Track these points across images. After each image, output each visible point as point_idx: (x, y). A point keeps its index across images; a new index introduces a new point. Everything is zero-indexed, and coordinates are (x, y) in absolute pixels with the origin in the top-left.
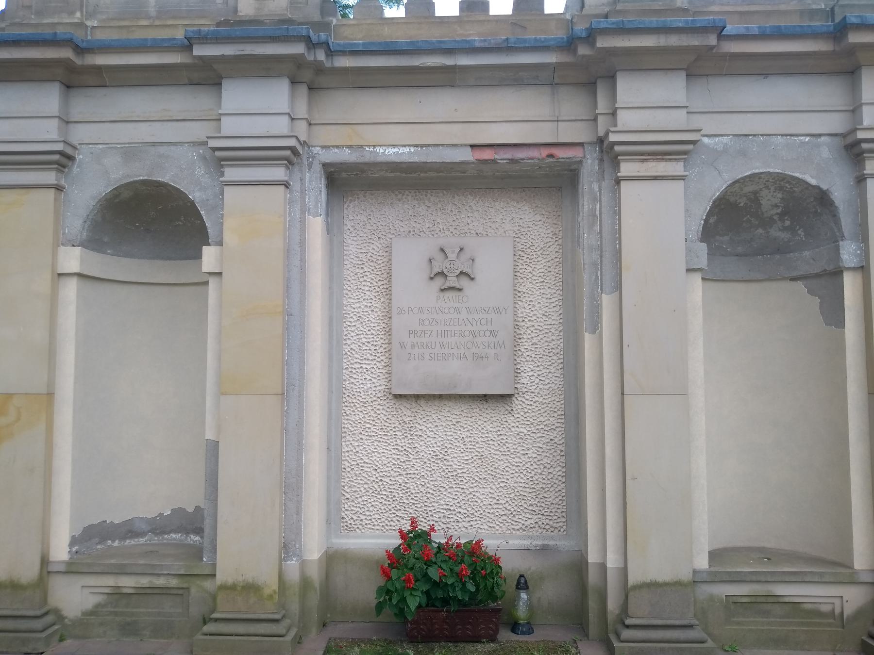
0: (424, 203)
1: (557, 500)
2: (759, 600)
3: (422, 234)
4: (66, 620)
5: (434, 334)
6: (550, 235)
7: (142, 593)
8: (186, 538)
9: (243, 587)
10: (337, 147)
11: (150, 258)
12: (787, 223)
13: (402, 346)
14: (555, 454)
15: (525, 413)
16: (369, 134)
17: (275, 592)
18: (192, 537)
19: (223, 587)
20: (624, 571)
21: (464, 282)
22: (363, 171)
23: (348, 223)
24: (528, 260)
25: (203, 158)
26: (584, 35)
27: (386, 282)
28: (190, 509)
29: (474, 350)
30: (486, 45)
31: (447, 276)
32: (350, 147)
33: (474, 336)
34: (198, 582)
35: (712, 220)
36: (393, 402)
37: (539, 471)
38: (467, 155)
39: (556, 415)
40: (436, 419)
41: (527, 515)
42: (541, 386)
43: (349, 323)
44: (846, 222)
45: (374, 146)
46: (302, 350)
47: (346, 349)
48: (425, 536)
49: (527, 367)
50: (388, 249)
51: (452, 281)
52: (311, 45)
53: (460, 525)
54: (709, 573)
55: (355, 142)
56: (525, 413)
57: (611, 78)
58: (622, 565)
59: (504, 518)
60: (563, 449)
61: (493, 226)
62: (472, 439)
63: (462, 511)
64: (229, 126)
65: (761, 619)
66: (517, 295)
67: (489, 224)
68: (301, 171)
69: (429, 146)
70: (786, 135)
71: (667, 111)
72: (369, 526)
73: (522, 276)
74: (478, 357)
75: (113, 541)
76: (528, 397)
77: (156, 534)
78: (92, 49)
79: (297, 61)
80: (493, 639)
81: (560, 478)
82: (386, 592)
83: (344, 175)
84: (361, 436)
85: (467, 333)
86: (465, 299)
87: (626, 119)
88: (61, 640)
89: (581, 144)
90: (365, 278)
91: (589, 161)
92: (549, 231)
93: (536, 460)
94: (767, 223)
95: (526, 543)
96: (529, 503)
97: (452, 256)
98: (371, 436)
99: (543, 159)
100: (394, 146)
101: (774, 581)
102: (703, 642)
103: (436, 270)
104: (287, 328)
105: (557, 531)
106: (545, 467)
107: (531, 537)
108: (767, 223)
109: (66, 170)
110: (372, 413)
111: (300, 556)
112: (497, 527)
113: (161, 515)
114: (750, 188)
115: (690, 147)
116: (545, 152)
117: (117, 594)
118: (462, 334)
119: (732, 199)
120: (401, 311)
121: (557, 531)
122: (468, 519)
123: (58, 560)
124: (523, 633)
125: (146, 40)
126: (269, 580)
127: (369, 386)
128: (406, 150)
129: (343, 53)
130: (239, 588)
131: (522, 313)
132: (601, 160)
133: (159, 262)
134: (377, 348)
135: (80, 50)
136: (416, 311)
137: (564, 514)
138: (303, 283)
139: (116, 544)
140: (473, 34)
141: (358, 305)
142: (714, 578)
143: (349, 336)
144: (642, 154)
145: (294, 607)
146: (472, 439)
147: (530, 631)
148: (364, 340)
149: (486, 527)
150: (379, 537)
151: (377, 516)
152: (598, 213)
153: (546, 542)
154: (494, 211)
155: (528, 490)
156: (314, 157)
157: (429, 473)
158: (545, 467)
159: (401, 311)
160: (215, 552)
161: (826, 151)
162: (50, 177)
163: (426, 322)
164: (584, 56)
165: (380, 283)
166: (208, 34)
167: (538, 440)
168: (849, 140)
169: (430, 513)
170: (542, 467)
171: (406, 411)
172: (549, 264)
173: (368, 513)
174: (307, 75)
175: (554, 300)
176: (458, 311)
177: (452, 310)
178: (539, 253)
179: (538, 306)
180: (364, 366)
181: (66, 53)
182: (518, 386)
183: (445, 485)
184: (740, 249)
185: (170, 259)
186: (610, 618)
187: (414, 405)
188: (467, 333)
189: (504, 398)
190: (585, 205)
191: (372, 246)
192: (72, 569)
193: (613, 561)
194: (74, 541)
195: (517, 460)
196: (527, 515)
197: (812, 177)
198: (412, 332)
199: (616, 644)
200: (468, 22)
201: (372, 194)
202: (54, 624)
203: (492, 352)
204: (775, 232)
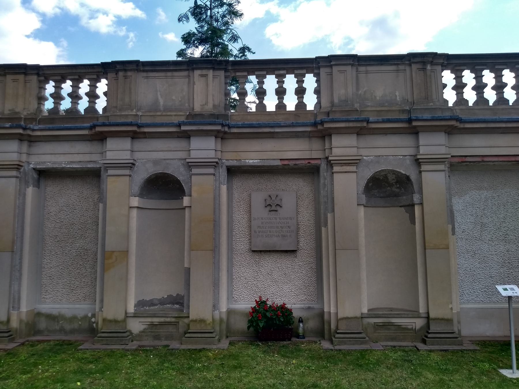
0: (263, 179)
1: (314, 290)
2: (386, 324)
3: (262, 190)
4: (133, 334)
5: (267, 227)
6: (310, 190)
7: (161, 324)
8: (173, 306)
9: (199, 321)
10: (231, 160)
11: (159, 199)
12: (398, 186)
13: (255, 232)
14: (313, 272)
15: (301, 257)
16: (243, 155)
17: (211, 322)
18: (175, 306)
19: (192, 321)
20: (337, 314)
21: (278, 208)
22: (240, 167)
23: (235, 186)
24: (302, 200)
25: (183, 164)
26: (320, 122)
27: (249, 208)
28: (175, 295)
29: (282, 233)
30: (285, 125)
31: (271, 206)
32: (236, 160)
33: (282, 228)
34: (182, 320)
35: (370, 185)
36: (252, 253)
37: (307, 279)
38: (278, 163)
39: (313, 258)
40: (268, 259)
41: (303, 296)
42: (307, 247)
43: (235, 224)
44: (416, 187)
45: (245, 160)
46: (219, 234)
47: (234, 233)
48: (265, 303)
49: (302, 240)
50: (250, 196)
51: (274, 208)
52: (223, 125)
53: (278, 299)
54: (367, 314)
55: (238, 158)
56: (301, 257)
57: (330, 136)
58: (336, 312)
59: (294, 297)
60: (316, 270)
61: (289, 187)
62: (282, 267)
63: (278, 294)
64: (193, 154)
65: (387, 331)
66: (298, 213)
67: (287, 186)
68: (219, 169)
69: (265, 159)
70: (394, 156)
71: (350, 148)
72: (243, 300)
73: (300, 205)
74: (284, 236)
75: (146, 307)
76: (302, 251)
77: (162, 305)
78: (143, 126)
79: (218, 131)
80: (290, 340)
81: (315, 281)
82: (250, 321)
83: (233, 169)
84: (240, 266)
85: (279, 227)
86: (278, 214)
87: (335, 151)
88: (132, 341)
89: (320, 159)
90: (241, 206)
91: (323, 165)
92: (310, 189)
93: (306, 275)
94: (391, 185)
95: (302, 306)
96: (303, 291)
97: (273, 198)
98: (244, 266)
99: (306, 164)
100: (252, 160)
101: (390, 317)
102: (365, 338)
103: (268, 204)
104: (214, 226)
105: (313, 301)
106: (309, 277)
107: (304, 304)
108: (391, 185)
109: (132, 169)
110: (244, 257)
111: (219, 310)
112: (291, 300)
113: (163, 297)
114: (383, 173)
115: (358, 161)
116: (307, 161)
117: (152, 325)
118: (277, 227)
119: (377, 177)
120: (255, 219)
121: (313, 301)
122: (280, 297)
123: (130, 312)
124: (301, 338)
125: (163, 123)
126: (209, 318)
127: (243, 247)
128: (257, 161)
129: (234, 127)
130: (198, 321)
131: (300, 219)
132: (327, 165)
133: (162, 201)
134: (246, 233)
135: (139, 126)
136: (260, 219)
137: (316, 295)
138: (220, 210)
139: (147, 308)
140: (280, 119)
141: (238, 217)
142: (369, 316)
143: (235, 228)
144: (341, 164)
145: (217, 328)
146: (282, 267)
147: (304, 338)
148: (241, 230)
149: (287, 300)
150: (247, 304)
151: (246, 296)
152: (326, 183)
153: (310, 306)
154: (288, 181)
155: (303, 286)
156: (223, 164)
157: (266, 280)
158: (309, 277)
159: (255, 219)
160: (189, 309)
161: (408, 161)
162: (127, 172)
163: (264, 223)
164: (320, 129)
165: (247, 208)
166: (186, 122)
167: (306, 267)
168: (416, 158)
169: (266, 295)
170: (308, 277)
171: (257, 257)
172: (310, 201)
173: (243, 295)
174: (221, 135)
175: (312, 214)
176: (276, 219)
177: (274, 218)
178: (306, 197)
179: (306, 216)
180: (241, 240)
181: (135, 128)
182: (299, 247)
183: (272, 285)
184: (382, 195)
185: (166, 199)
186: (332, 331)
187: (260, 254)
188: (279, 227)
189: (294, 252)
190: (322, 181)
191: (243, 195)
192: (135, 316)
193: (333, 310)
194: (135, 306)
195: (299, 275)
196: (303, 296)
197: (403, 171)
198: (259, 227)
199: (334, 339)
200: (279, 114)
201: (243, 175)
202: (129, 336)
203: (289, 234)
204: (394, 189)
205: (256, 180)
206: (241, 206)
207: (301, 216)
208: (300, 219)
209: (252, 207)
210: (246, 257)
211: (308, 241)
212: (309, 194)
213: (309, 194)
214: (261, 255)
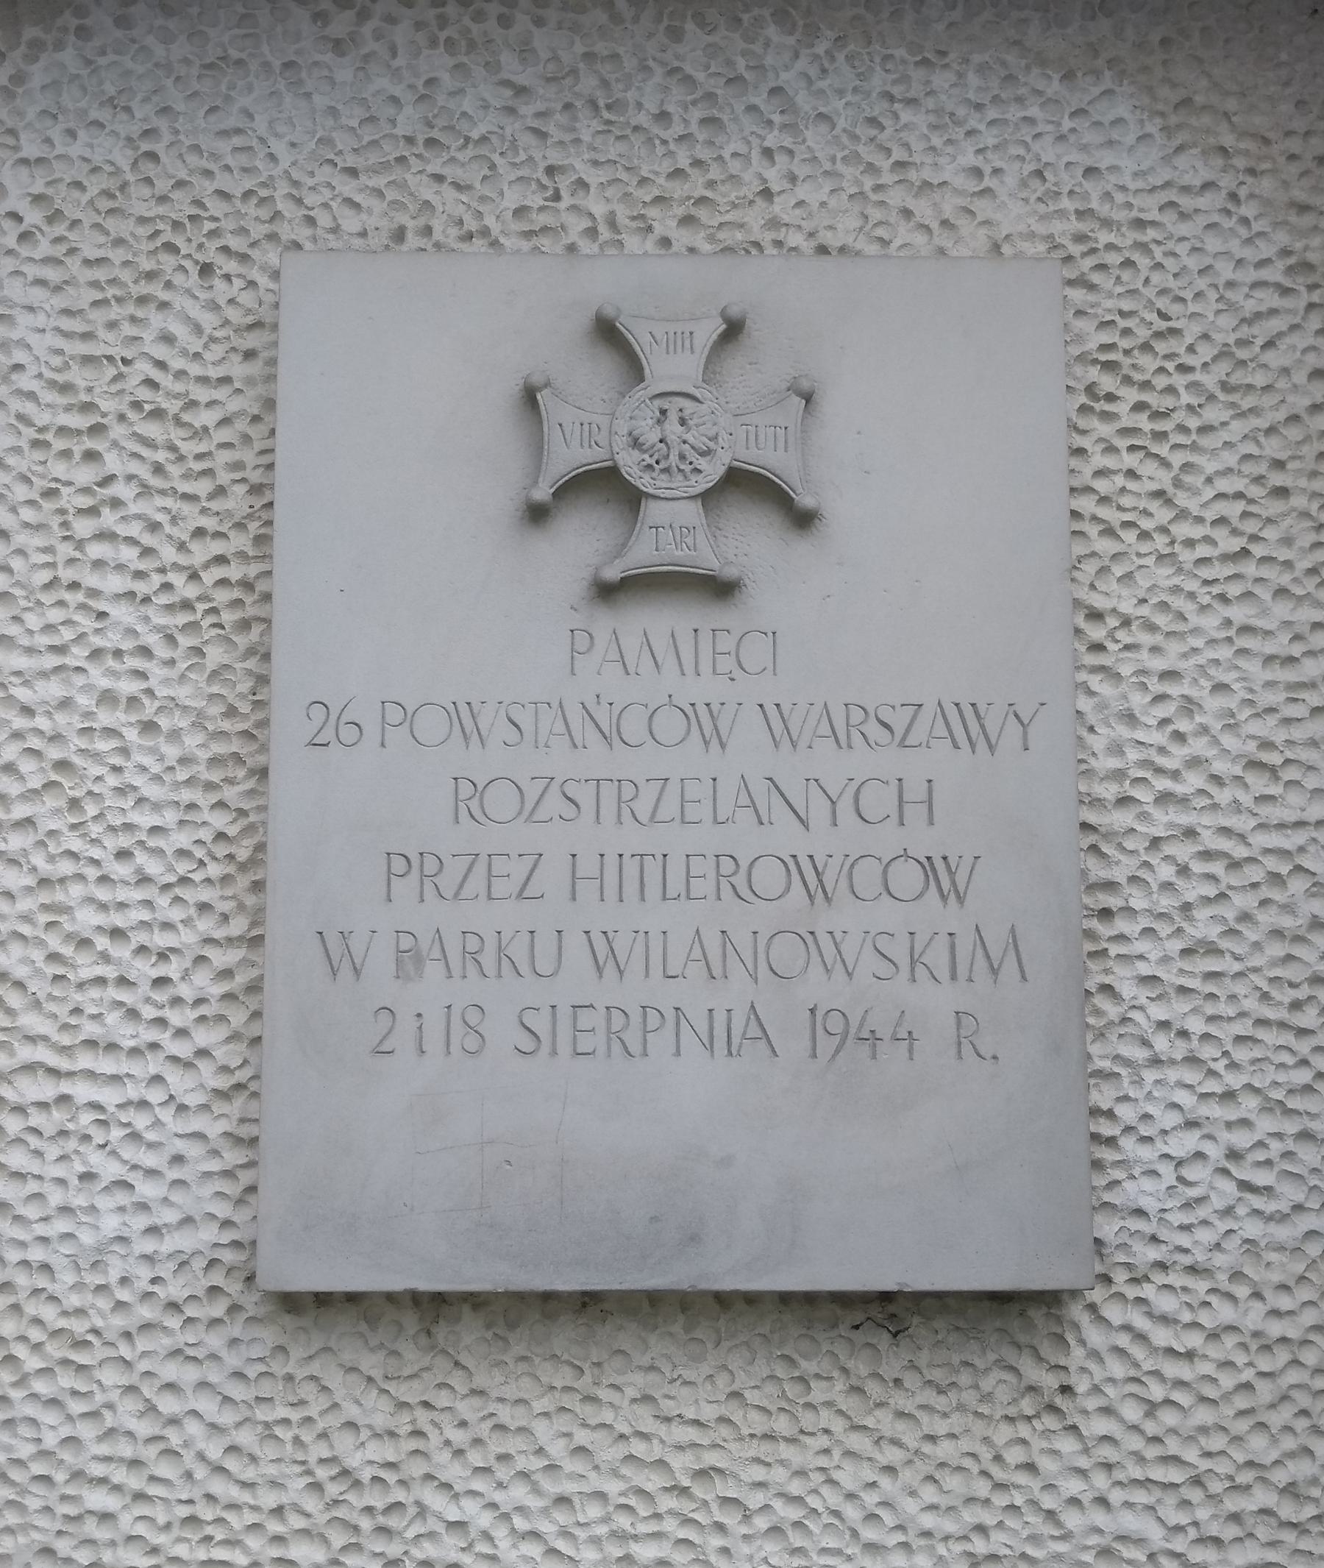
0: (492, 67)
5: (552, 879)
6: (1274, 274)
15: (1152, 1408)
24: (1143, 421)
27: (240, 541)
33: (820, 893)
40: (557, 1449)
42: (1253, 1229)
61: (922, 208)
67: (896, 197)
76: (1166, 1304)
85: (769, 877)
86: (756, 653)
90: (109, 518)
92: (1266, 250)
127: (111, 1224)
131: (1116, 749)
134: (172, 969)
136: (432, 725)
148: (87, 919)
163: (501, 801)
165: (201, 552)
177: (669, 725)
178: (1209, 381)
179: (1214, 703)
180: (82, 1091)
182: (1108, 1228)
187: (413, 1356)
188: (769, 877)
191: (157, 320)
205: (383, 83)
206: (109, 518)
207: (1138, 700)
208: (1116, 749)
209: (282, 497)
210: (168, 1405)
211: (1266, 1124)
212: (1261, 332)
213: (1261, 332)
214: (442, 1363)
